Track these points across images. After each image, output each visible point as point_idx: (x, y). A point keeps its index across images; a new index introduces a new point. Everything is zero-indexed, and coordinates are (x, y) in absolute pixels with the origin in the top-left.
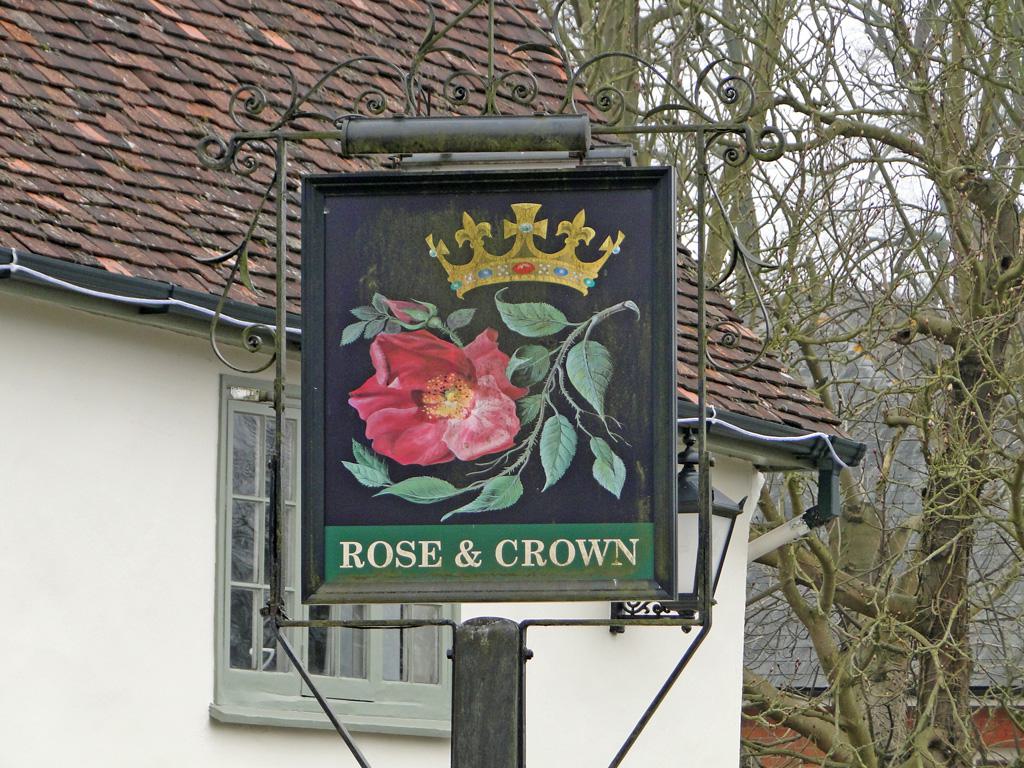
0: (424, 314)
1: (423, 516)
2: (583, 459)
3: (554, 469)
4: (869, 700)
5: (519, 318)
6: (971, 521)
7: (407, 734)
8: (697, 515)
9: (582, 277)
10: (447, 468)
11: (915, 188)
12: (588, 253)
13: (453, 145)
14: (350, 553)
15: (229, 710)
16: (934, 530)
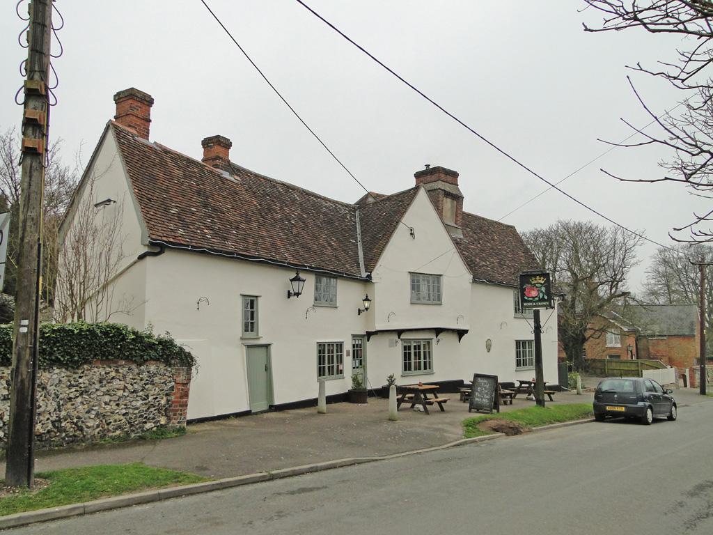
1: (531, 301)
2: (543, 296)
3: (541, 297)
4: (567, 315)
6: (42, 110)
9: (543, 282)
10: (533, 297)
11: (569, 274)
13: (531, 272)
16: (572, 301)
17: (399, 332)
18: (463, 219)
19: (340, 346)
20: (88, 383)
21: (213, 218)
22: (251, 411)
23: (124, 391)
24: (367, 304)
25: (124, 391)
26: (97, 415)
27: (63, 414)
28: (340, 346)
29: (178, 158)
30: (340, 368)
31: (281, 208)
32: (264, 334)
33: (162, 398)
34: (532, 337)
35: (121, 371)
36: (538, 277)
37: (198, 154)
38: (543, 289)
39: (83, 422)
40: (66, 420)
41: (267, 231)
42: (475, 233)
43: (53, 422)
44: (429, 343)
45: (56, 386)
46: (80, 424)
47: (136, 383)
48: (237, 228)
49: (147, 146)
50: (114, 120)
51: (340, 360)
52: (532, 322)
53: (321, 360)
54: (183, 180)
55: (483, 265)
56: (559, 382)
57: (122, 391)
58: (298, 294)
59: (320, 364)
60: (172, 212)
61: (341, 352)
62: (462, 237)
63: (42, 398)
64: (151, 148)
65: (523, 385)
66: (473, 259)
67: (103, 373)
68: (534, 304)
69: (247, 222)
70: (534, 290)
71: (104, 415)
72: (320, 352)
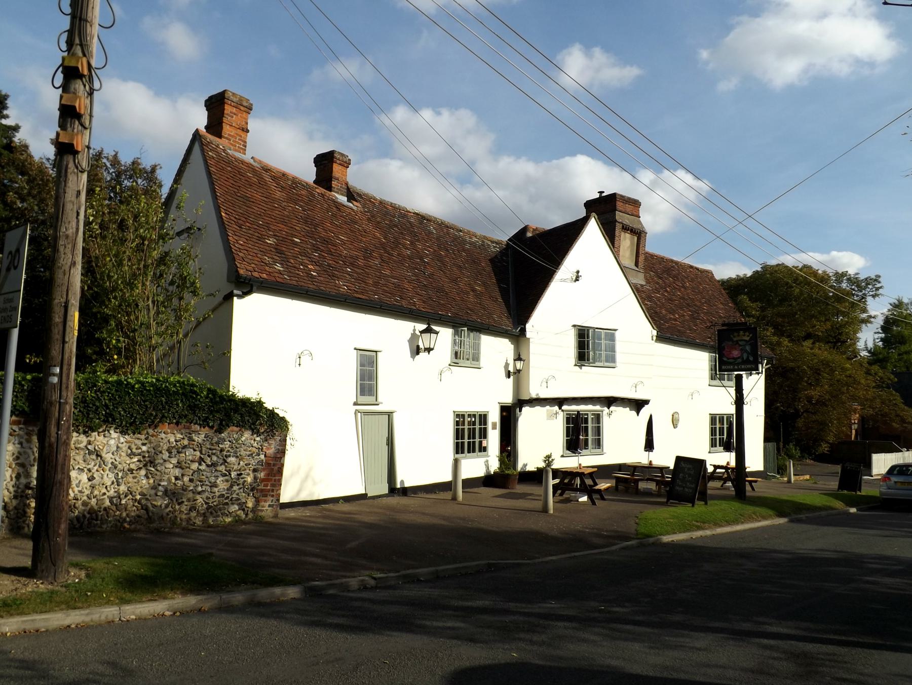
0: (731, 343)
3: (745, 358)
5: (741, 343)
7: (459, 466)
8: (281, 501)
9: (748, 339)
10: (734, 358)
12: (748, 336)
14: (723, 367)
15: (711, 384)
17: (560, 402)
18: (646, 259)
19: (483, 418)
20: (153, 451)
21: (322, 251)
22: (366, 494)
23: (200, 464)
24: (519, 365)
25: (200, 464)
26: (166, 492)
27: (123, 488)
28: (483, 418)
29: (280, 178)
30: (484, 444)
31: (412, 243)
32: (386, 399)
33: (248, 474)
34: (732, 410)
35: (196, 438)
36: (741, 333)
37: (308, 173)
38: (748, 348)
39: (147, 499)
40: (126, 496)
41: (392, 270)
42: (661, 278)
43: (111, 499)
44: (598, 418)
45: (113, 454)
46: (143, 502)
47: (214, 454)
48: (352, 265)
49: (243, 162)
50: (205, 131)
51: (484, 434)
52: (733, 391)
53: (459, 434)
54: (285, 204)
55: (670, 318)
56: (765, 466)
57: (197, 464)
58: (429, 350)
59: (457, 438)
60: (269, 242)
61: (485, 424)
62: (644, 283)
63: (96, 468)
64: (249, 165)
65: (718, 470)
66: (658, 310)
67: (172, 440)
68: (736, 367)
69: (365, 258)
70: (736, 349)
71: (175, 493)
72: (457, 423)
